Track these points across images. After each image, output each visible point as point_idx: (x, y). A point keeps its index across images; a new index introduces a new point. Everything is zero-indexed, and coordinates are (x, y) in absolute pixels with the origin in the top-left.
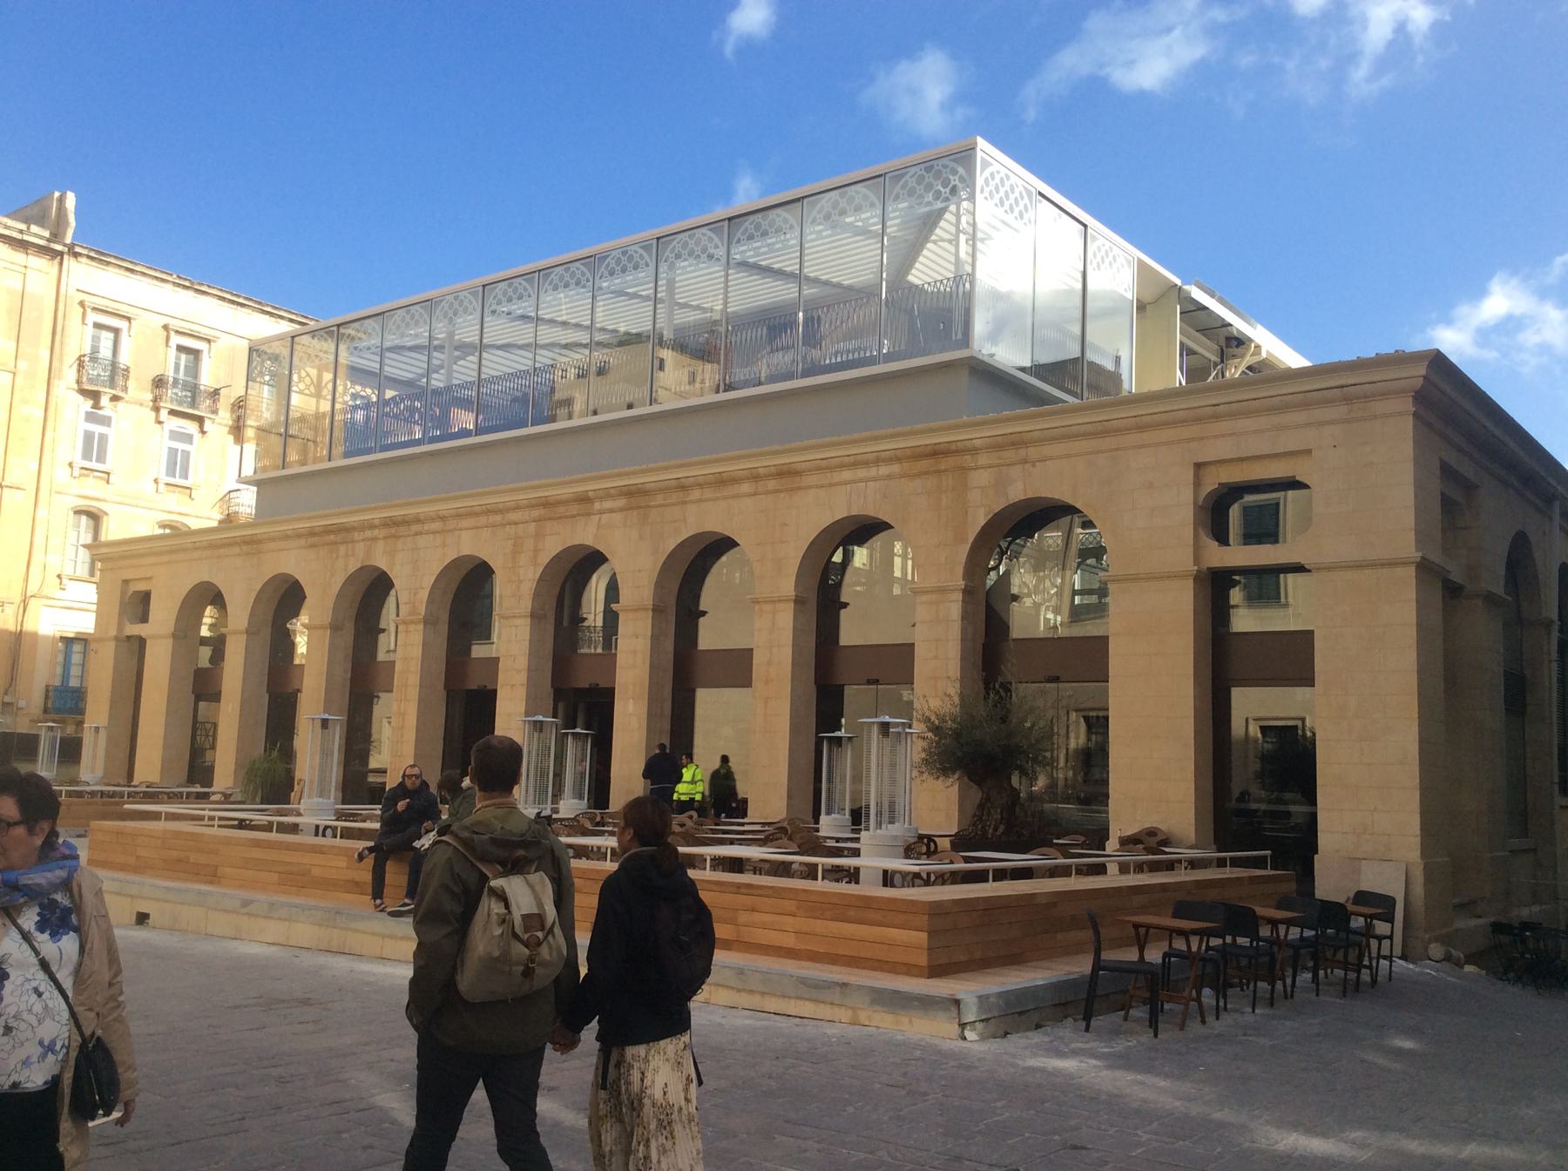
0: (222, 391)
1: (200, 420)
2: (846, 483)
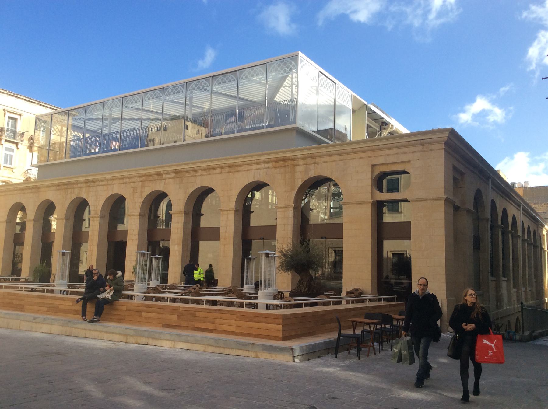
0: (25, 134)
2: (253, 170)
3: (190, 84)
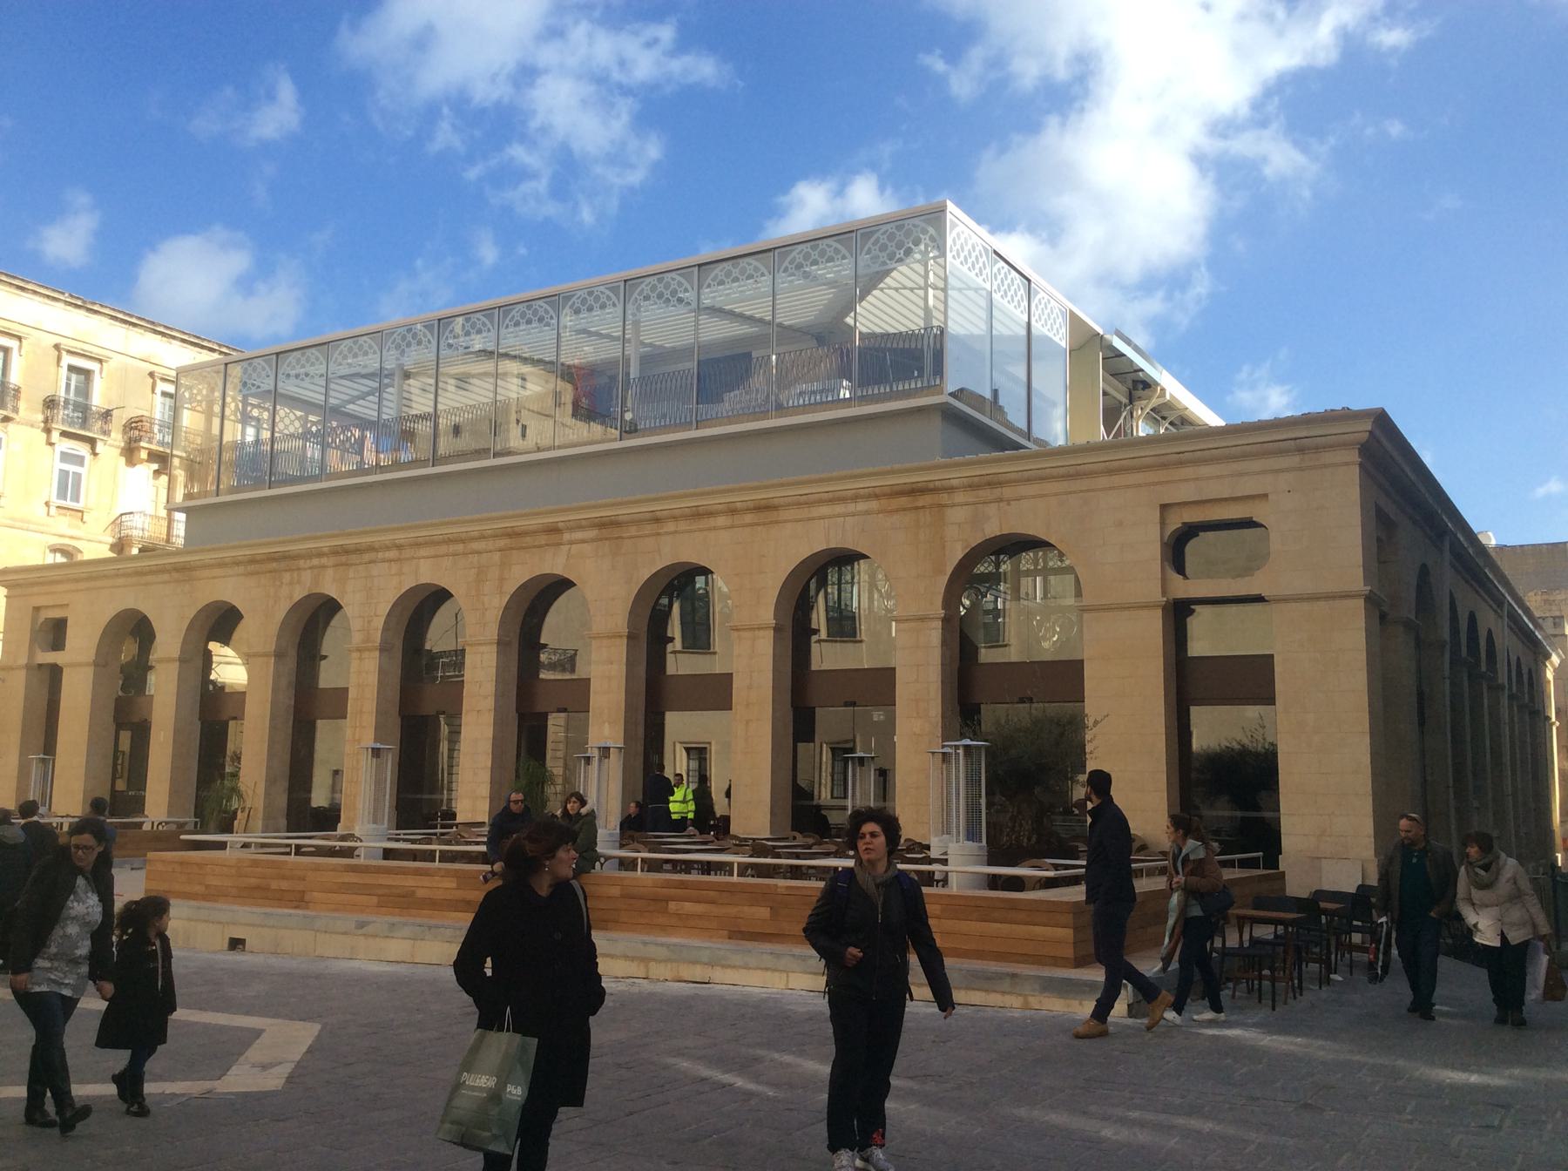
0: (115, 413)
1: (92, 442)
3: (636, 283)
